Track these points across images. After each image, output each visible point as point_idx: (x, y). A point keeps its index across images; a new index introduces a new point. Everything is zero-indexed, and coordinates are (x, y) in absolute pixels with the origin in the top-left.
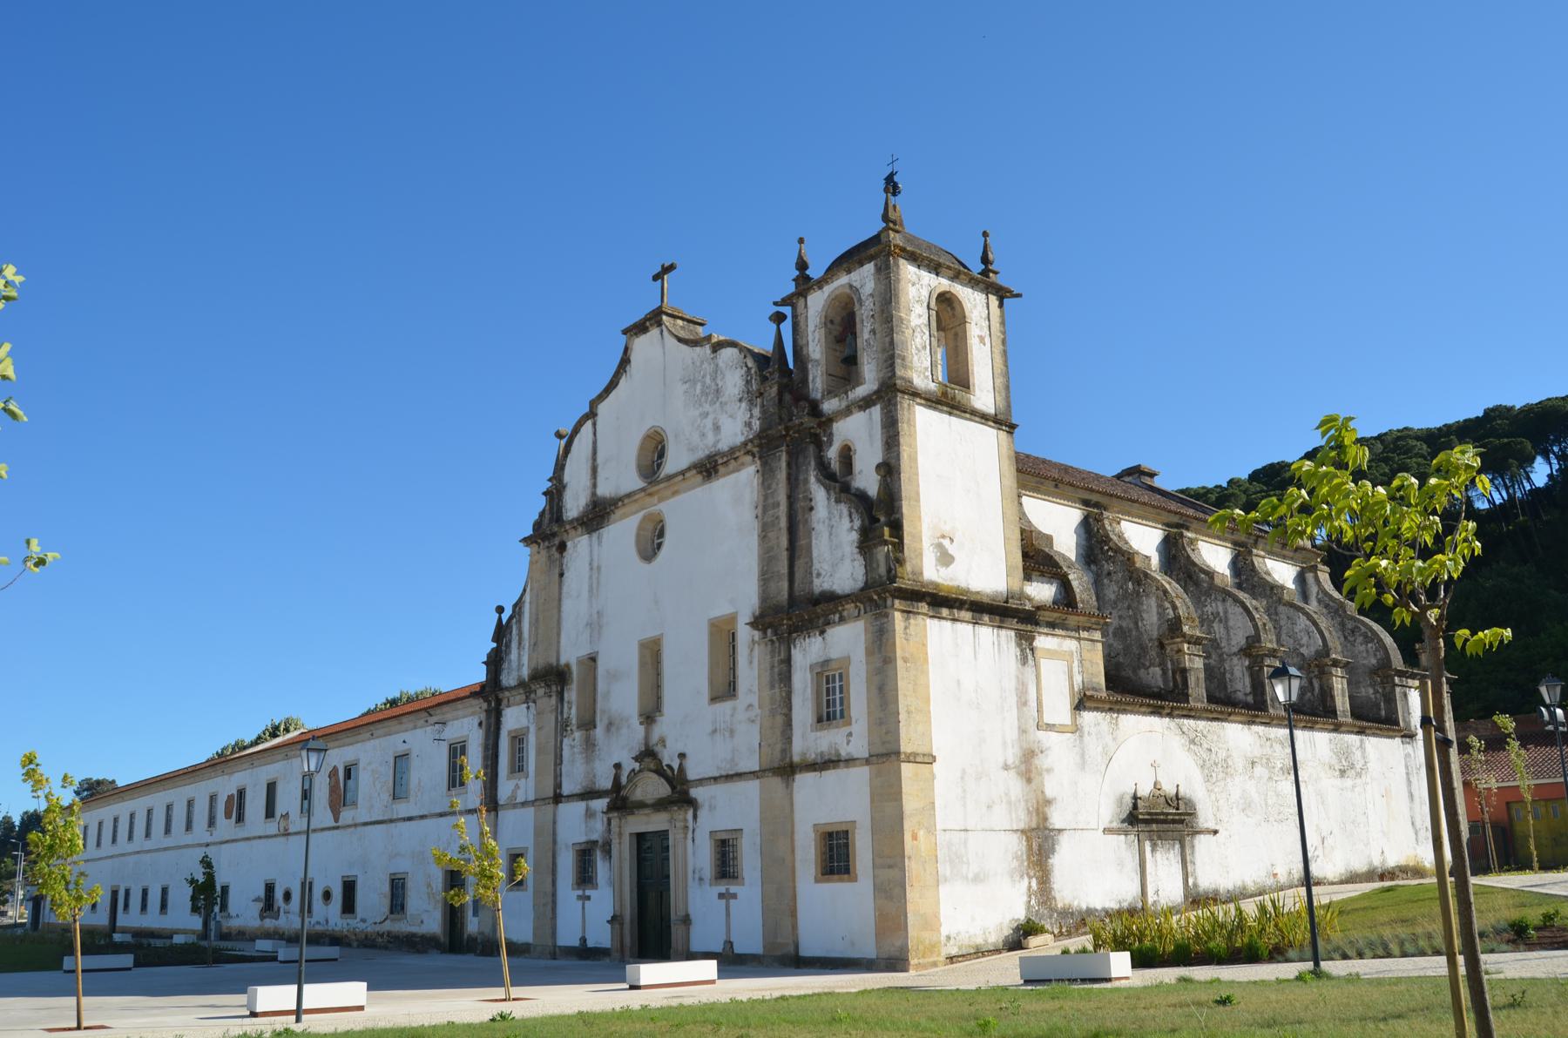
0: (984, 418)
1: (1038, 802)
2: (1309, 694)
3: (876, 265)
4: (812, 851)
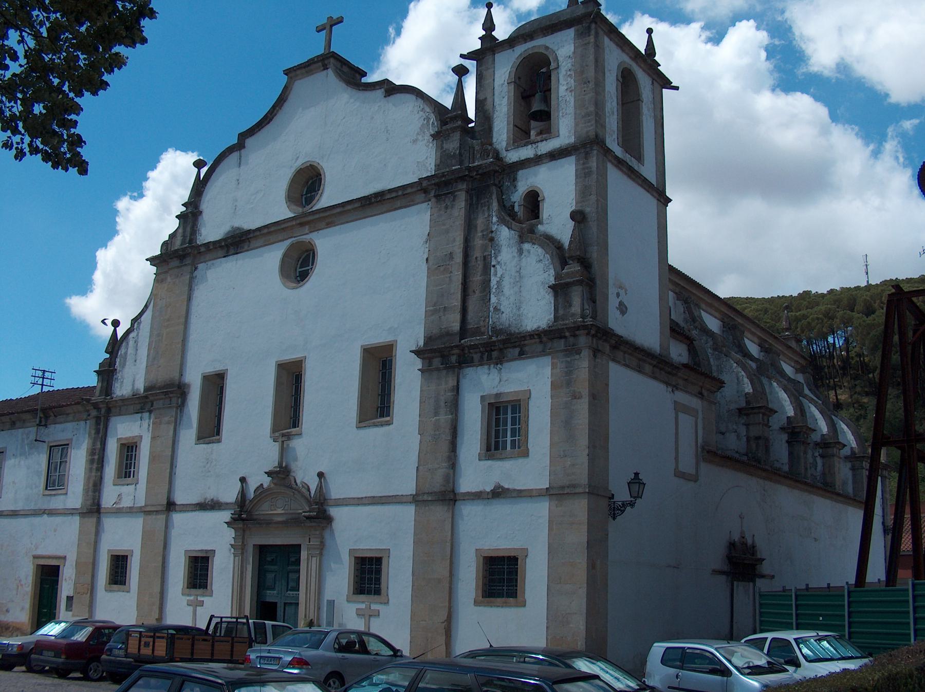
3: (577, 31)
4: (215, 574)
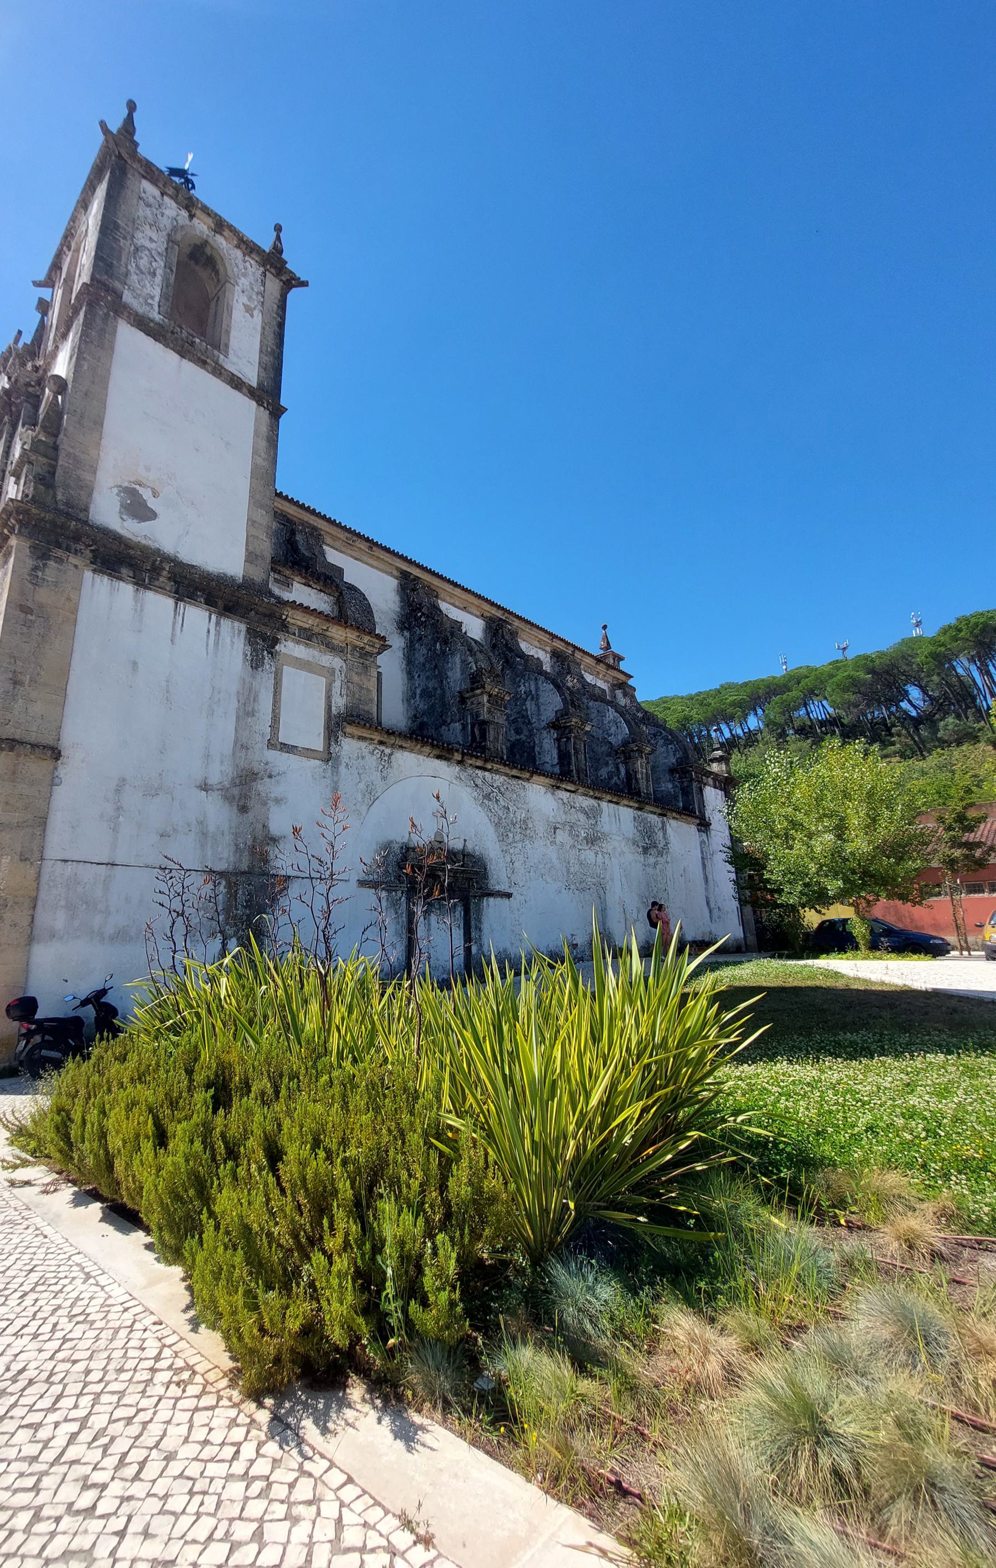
0: (236, 383)
1: (255, 839)
2: (616, 778)
